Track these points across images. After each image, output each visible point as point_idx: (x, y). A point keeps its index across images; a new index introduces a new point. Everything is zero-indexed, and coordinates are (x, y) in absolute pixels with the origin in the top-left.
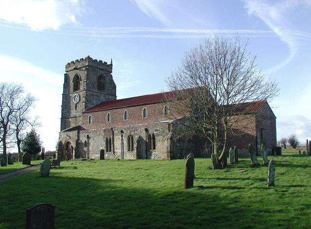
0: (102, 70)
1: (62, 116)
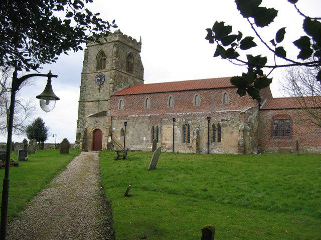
0: (131, 47)
1: (80, 98)
